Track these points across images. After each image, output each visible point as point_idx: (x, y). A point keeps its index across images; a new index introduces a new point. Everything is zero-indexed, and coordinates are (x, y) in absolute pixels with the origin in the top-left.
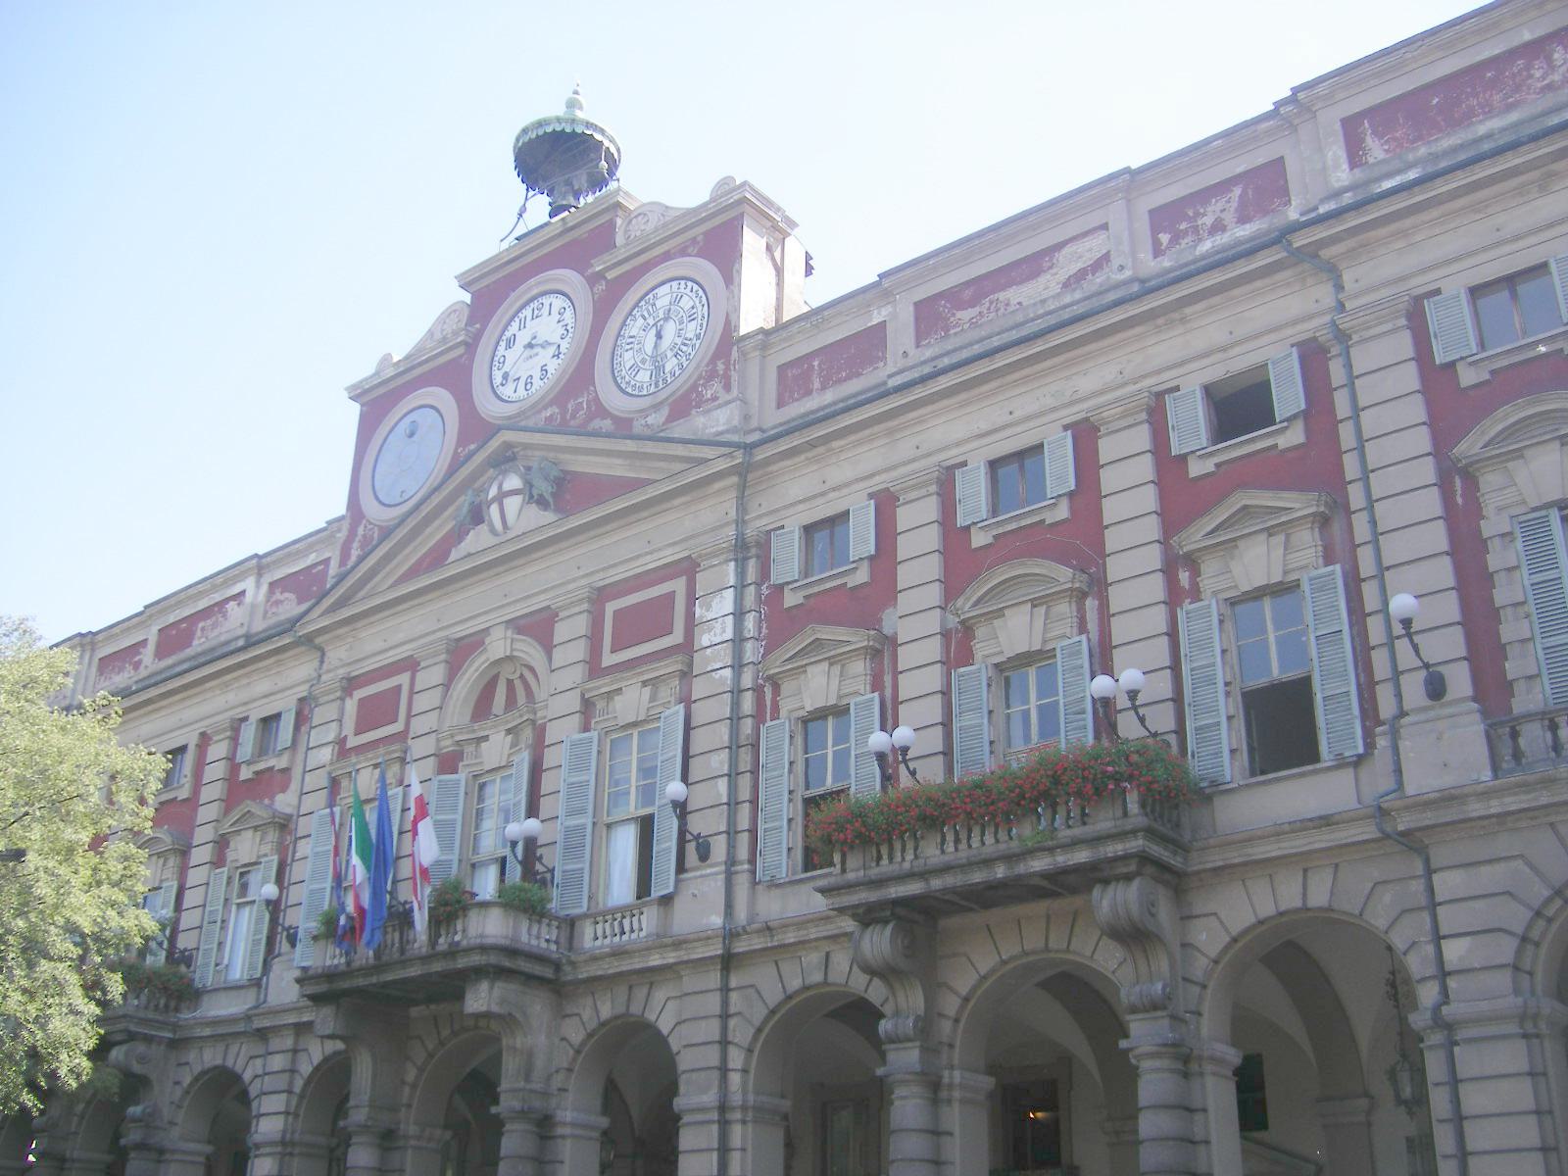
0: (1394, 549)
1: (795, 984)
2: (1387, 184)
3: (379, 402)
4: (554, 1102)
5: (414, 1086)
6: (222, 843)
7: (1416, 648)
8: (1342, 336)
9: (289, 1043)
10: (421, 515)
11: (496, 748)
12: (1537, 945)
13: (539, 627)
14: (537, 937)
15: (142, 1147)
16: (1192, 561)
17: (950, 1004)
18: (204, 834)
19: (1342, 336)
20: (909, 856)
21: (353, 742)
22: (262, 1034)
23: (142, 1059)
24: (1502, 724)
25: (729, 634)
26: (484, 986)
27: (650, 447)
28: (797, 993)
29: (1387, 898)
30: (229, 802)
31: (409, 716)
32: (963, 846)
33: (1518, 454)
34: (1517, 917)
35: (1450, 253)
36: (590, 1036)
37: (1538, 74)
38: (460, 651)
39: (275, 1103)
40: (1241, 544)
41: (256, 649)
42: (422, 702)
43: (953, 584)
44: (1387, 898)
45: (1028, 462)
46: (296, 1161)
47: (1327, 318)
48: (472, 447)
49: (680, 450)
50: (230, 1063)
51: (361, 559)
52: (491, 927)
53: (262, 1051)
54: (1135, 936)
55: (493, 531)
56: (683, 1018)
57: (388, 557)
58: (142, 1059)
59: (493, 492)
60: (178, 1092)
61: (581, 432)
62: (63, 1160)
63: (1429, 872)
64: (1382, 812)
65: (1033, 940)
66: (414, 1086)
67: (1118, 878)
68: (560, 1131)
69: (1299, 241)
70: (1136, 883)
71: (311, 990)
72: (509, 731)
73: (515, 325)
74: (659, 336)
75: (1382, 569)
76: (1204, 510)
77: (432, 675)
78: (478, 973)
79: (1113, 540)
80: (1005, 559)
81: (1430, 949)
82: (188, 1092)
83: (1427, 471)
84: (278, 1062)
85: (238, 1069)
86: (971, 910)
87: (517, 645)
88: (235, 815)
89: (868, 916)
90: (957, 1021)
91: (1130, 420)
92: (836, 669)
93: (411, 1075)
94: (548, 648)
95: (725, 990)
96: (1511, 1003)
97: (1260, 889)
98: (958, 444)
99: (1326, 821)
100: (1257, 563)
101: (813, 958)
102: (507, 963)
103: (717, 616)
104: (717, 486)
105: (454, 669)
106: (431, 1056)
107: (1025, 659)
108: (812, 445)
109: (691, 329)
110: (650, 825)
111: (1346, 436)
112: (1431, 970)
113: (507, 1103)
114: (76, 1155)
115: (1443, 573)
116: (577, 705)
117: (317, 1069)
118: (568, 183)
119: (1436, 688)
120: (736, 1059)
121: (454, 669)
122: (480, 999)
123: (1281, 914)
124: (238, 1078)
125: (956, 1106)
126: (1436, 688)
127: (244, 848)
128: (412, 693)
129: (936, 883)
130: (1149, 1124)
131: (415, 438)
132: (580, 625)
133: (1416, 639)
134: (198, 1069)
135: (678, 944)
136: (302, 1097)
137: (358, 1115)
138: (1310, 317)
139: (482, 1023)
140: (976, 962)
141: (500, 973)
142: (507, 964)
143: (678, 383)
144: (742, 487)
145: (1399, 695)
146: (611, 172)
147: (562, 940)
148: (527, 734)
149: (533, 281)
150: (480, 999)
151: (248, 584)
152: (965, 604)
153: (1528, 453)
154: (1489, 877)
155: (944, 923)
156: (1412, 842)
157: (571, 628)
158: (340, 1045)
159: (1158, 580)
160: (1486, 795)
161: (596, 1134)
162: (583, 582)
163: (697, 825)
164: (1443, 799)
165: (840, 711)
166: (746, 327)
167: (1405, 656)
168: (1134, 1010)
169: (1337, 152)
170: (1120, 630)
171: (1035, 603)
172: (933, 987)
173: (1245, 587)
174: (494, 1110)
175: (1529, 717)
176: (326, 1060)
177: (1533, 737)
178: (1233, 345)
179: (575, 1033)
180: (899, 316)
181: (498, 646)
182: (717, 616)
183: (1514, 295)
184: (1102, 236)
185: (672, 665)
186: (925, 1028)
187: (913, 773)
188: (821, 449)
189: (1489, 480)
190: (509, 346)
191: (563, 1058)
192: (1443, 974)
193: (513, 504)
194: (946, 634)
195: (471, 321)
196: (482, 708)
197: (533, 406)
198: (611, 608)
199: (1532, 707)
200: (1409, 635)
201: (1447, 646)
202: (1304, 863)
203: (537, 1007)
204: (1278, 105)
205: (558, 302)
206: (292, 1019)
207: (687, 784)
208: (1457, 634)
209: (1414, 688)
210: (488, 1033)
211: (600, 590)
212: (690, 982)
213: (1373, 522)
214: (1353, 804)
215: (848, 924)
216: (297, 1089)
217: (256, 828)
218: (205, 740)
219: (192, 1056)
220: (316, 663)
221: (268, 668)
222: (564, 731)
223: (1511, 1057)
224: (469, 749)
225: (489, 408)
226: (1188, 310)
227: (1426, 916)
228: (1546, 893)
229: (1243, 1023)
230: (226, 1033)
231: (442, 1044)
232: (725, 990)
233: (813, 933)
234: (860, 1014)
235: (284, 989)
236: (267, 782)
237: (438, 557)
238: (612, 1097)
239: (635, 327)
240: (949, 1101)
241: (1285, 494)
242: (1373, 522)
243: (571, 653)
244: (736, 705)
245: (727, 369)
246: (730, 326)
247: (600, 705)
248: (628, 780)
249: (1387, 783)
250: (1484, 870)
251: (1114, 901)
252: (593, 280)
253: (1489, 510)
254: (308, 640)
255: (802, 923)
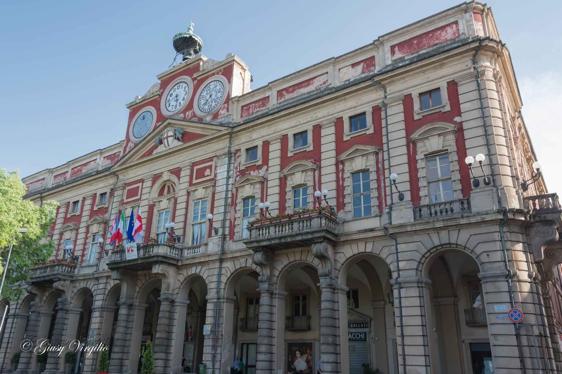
0: (393, 162)
1: (238, 267)
2: (401, 65)
3: (135, 109)
4: (175, 297)
5: (138, 293)
6: (88, 227)
7: (396, 187)
8: (385, 105)
9: (105, 281)
10: (145, 141)
11: (164, 204)
12: (423, 264)
13: (177, 172)
14: (173, 254)
15: (62, 309)
16: (343, 162)
17: (276, 273)
18: (83, 225)
19: (385, 105)
20: (267, 235)
21: (125, 201)
22: (97, 279)
23: (62, 286)
24: (417, 207)
25: (224, 197)
26: (157, 266)
27: (207, 126)
28: (239, 269)
29: (386, 250)
30: (91, 216)
31: (141, 195)
32: (281, 232)
33: (427, 138)
34: (418, 256)
35: (415, 84)
36: (186, 279)
37: (443, 35)
38: (156, 178)
39: (100, 297)
40: (355, 159)
41: (99, 174)
42: (145, 191)
43: (283, 166)
44: (386, 250)
45: (303, 135)
46: (105, 313)
47: (382, 100)
48: (160, 123)
49: (215, 127)
50: (88, 286)
51: (129, 152)
52: (162, 250)
53: (97, 283)
54: (322, 257)
55: (165, 146)
56: (209, 275)
57: (136, 152)
58: (62, 286)
59: (165, 136)
60: (73, 294)
61: (190, 121)
62: (39, 313)
63: (397, 244)
64: (386, 229)
65: (298, 257)
66: (138, 293)
67: (318, 242)
68: (176, 304)
69: (376, 79)
70: (322, 244)
71: (111, 267)
72: (168, 199)
73: (173, 90)
74: (210, 96)
75: (390, 166)
76: (346, 150)
77: (148, 184)
78: (156, 262)
79: (323, 156)
80: (296, 160)
81: (396, 264)
82: (75, 294)
83: (404, 142)
84: (101, 286)
85: (90, 288)
86: (282, 249)
87: (171, 177)
88: (92, 219)
89: (256, 250)
90: (278, 277)
91: (329, 125)
92: (252, 186)
93: (137, 289)
94: (179, 178)
95: (221, 268)
96: (415, 279)
97: (354, 246)
98: (286, 129)
99: (372, 230)
100: (359, 164)
101: (243, 260)
102: (164, 260)
103: (222, 172)
104: (224, 137)
105: (154, 182)
106: (143, 284)
107: (300, 186)
108: (249, 128)
109: (219, 95)
110: (206, 221)
111: (384, 131)
112: (396, 269)
113: (162, 296)
114: (43, 312)
115: (406, 168)
116: (186, 193)
117: (112, 288)
118: (188, 52)
119: (401, 198)
120: (222, 286)
121: (154, 182)
122: (157, 269)
123: (360, 253)
124: (90, 291)
125: (277, 299)
126: (401, 198)
127: (95, 228)
128: (142, 188)
129: (273, 242)
130: (324, 305)
131: (146, 119)
132: (188, 172)
133: (397, 185)
134: (79, 288)
135: (209, 256)
136: (107, 295)
137: (122, 300)
138: (378, 100)
139: (157, 276)
140: (283, 263)
141: (162, 263)
142: (164, 260)
143: (216, 109)
144: (231, 138)
145: (392, 199)
146: (200, 49)
147: (179, 254)
148: (173, 200)
149: (177, 79)
150: (157, 269)
151: (98, 157)
152: (285, 171)
153: (430, 138)
154: (412, 246)
155: (276, 252)
156: (393, 237)
157: (185, 173)
158: (118, 282)
159: (334, 167)
160: (413, 225)
161: (186, 305)
162: (189, 161)
163: (215, 225)
164: (401, 226)
165: (253, 197)
166: (233, 95)
167: (394, 190)
168: (321, 276)
169: (389, 55)
170: (323, 179)
171: (303, 172)
172: (272, 269)
173: (355, 170)
174: (159, 299)
175: (424, 206)
176: (115, 285)
177: (425, 211)
178: (357, 106)
179: (182, 278)
180: (273, 94)
181: (165, 177)
182: (222, 172)
183: (430, 96)
184: (326, 75)
185: (209, 184)
186: (270, 279)
187: (270, 214)
188: (251, 129)
189: (419, 145)
190: (171, 96)
191: (178, 284)
192: (399, 270)
193: (170, 139)
194: (280, 179)
195: (161, 89)
196: (161, 193)
197: (177, 113)
198: (196, 168)
199: (425, 204)
200: (395, 184)
201: (405, 187)
202: (366, 240)
203: (171, 271)
204: (374, 41)
205: (184, 85)
206: (106, 275)
207: (213, 215)
208: (408, 184)
209: (396, 197)
210: (159, 279)
211: (193, 163)
212: (211, 266)
213: (389, 154)
214: (379, 226)
215: (252, 252)
216: (106, 293)
217: (98, 223)
218: (84, 199)
219: (77, 285)
220: (116, 179)
221: (102, 180)
222: (182, 199)
223: (415, 292)
224: (157, 204)
225: (165, 113)
226: (346, 97)
227: (395, 255)
228: (426, 251)
229: (349, 280)
230: (87, 278)
231: (146, 281)
232: (221, 268)
233: (243, 254)
234: (255, 274)
235: (103, 266)
236: (103, 211)
237: (150, 152)
238: (191, 294)
239: (204, 94)
240: (275, 298)
241: (367, 146)
242: (389, 154)
243: (185, 179)
244: (226, 195)
245: (228, 106)
246: (229, 95)
247: (192, 193)
248: (198, 213)
249: (387, 221)
250: (411, 244)
251: (316, 248)
252: (194, 79)
253: (419, 153)
254: (114, 173)
255: (241, 251)
